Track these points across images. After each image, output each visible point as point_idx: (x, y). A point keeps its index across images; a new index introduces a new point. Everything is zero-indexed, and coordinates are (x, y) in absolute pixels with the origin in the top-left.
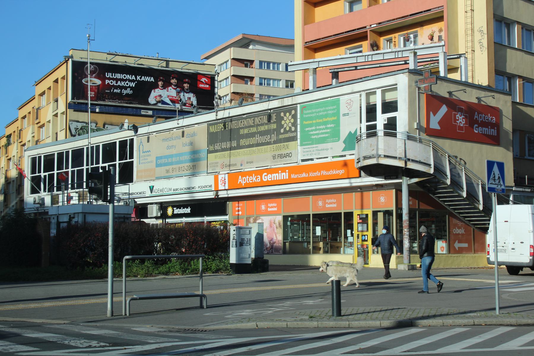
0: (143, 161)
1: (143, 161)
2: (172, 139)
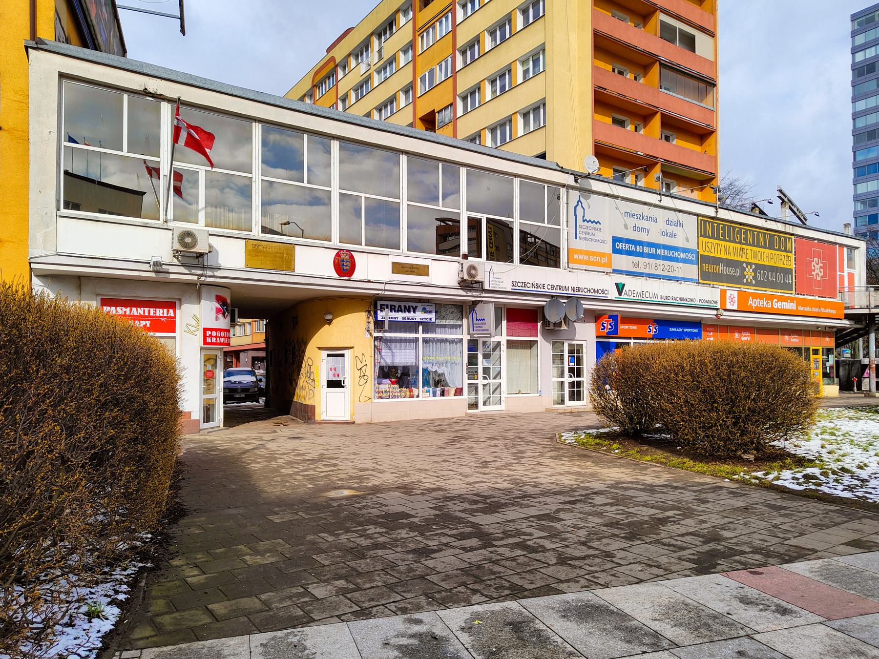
0: (584, 236)
1: (584, 236)
2: (643, 218)
